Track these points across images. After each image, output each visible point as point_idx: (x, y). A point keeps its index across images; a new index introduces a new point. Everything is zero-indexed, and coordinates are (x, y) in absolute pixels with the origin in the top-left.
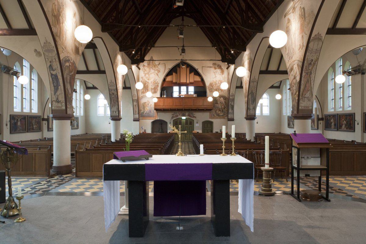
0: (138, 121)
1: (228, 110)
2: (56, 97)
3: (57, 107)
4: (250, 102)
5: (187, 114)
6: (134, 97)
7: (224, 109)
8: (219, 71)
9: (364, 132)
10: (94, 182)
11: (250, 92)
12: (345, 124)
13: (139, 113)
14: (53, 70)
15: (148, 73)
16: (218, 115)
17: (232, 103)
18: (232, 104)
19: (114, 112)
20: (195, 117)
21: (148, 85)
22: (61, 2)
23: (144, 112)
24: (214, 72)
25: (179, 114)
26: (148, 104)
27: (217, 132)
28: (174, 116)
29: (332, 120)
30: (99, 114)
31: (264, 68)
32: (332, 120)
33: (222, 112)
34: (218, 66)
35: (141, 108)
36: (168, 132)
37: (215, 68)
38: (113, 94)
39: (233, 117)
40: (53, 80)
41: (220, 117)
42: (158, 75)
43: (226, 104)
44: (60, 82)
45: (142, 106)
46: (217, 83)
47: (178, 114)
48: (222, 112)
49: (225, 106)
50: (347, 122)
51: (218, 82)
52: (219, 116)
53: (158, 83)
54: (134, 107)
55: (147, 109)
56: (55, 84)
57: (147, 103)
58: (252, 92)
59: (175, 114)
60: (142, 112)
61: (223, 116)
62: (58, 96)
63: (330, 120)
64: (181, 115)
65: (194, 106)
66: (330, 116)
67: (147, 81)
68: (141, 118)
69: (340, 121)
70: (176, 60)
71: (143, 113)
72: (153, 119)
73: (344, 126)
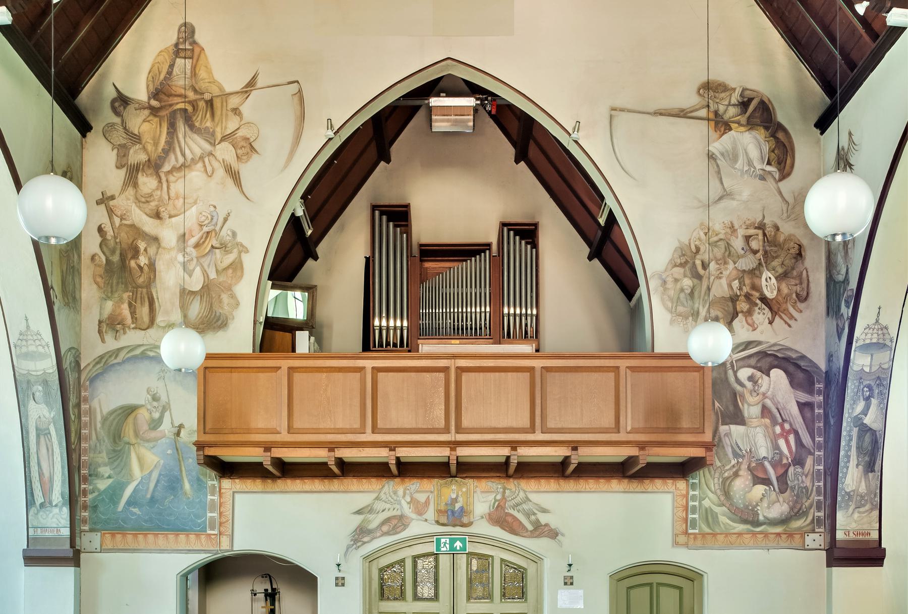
0: (74, 558)
1: (832, 474)
7: (799, 461)
13: (73, 501)
15: (154, 166)
17: (865, 412)
18: (867, 420)
20: (553, 534)
21: (152, 266)
22: (860, 467)
23: (122, 487)
26: (155, 424)
28: (375, 521)
33: (782, 491)
39: (875, 535)
41: (766, 535)
42: (235, 176)
45: (102, 434)
49: (806, 439)
51: (747, 238)
52: (757, 524)
53: (243, 249)
57: (143, 415)
61: (784, 521)
67: (149, 225)
68: (90, 540)
72: (205, 551)
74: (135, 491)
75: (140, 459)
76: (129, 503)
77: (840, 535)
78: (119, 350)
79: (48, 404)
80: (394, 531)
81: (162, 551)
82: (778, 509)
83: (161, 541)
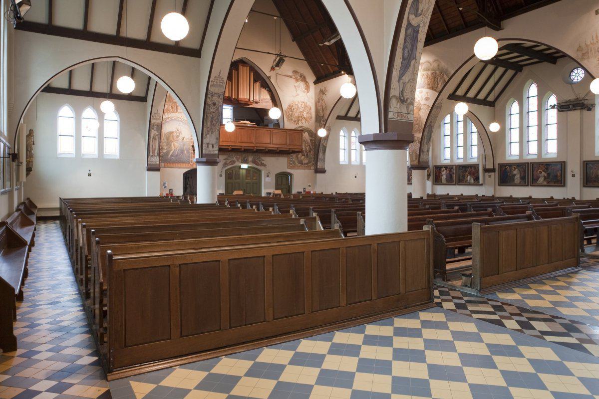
0: (158, 170)
2: (401, 86)
3: (399, 114)
4: (425, 140)
5: (250, 159)
6: (154, 119)
7: (310, 152)
8: (302, 85)
9: (584, 186)
10: (63, 321)
11: (428, 124)
12: (545, 177)
13: (159, 155)
14: (417, 15)
16: (301, 163)
19: (210, 146)
20: (265, 165)
23: (170, 151)
24: (295, 87)
25: (236, 158)
26: (178, 137)
27: (299, 193)
28: (228, 161)
29: (516, 172)
30: (61, 154)
31: (343, 114)
32: (516, 172)
33: (307, 157)
34: (301, 76)
35: (164, 144)
36: (263, 195)
37: (297, 80)
38: (214, 104)
40: (405, 42)
43: (312, 143)
44: (418, 50)
46: (300, 106)
47: (235, 159)
48: (307, 157)
49: (311, 147)
50: (549, 174)
52: (302, 164)
54: (151, 139)
55: (176, 146)
56: (406, 52)
57: (175, 134)
58: (430, 125)
59: (229, 158)
60: (164, 151)
61: (306, 164)
62: (404, 84)
63: (511, 171)
64: (240, 160)
65: (273, 144)
66: (511, 165)
69: (533, 172)
70: (268, 53)
71: (167, 153)
73: (541, 180)
74: (173, 153)
75: (174, 145)
76: (171, 156)
77: (318, 167)
78: (169, 118)
79: (157, 131)
80: (232, 164)
81: (179, 168)
82: (306, 161)
83: (179, 166)
